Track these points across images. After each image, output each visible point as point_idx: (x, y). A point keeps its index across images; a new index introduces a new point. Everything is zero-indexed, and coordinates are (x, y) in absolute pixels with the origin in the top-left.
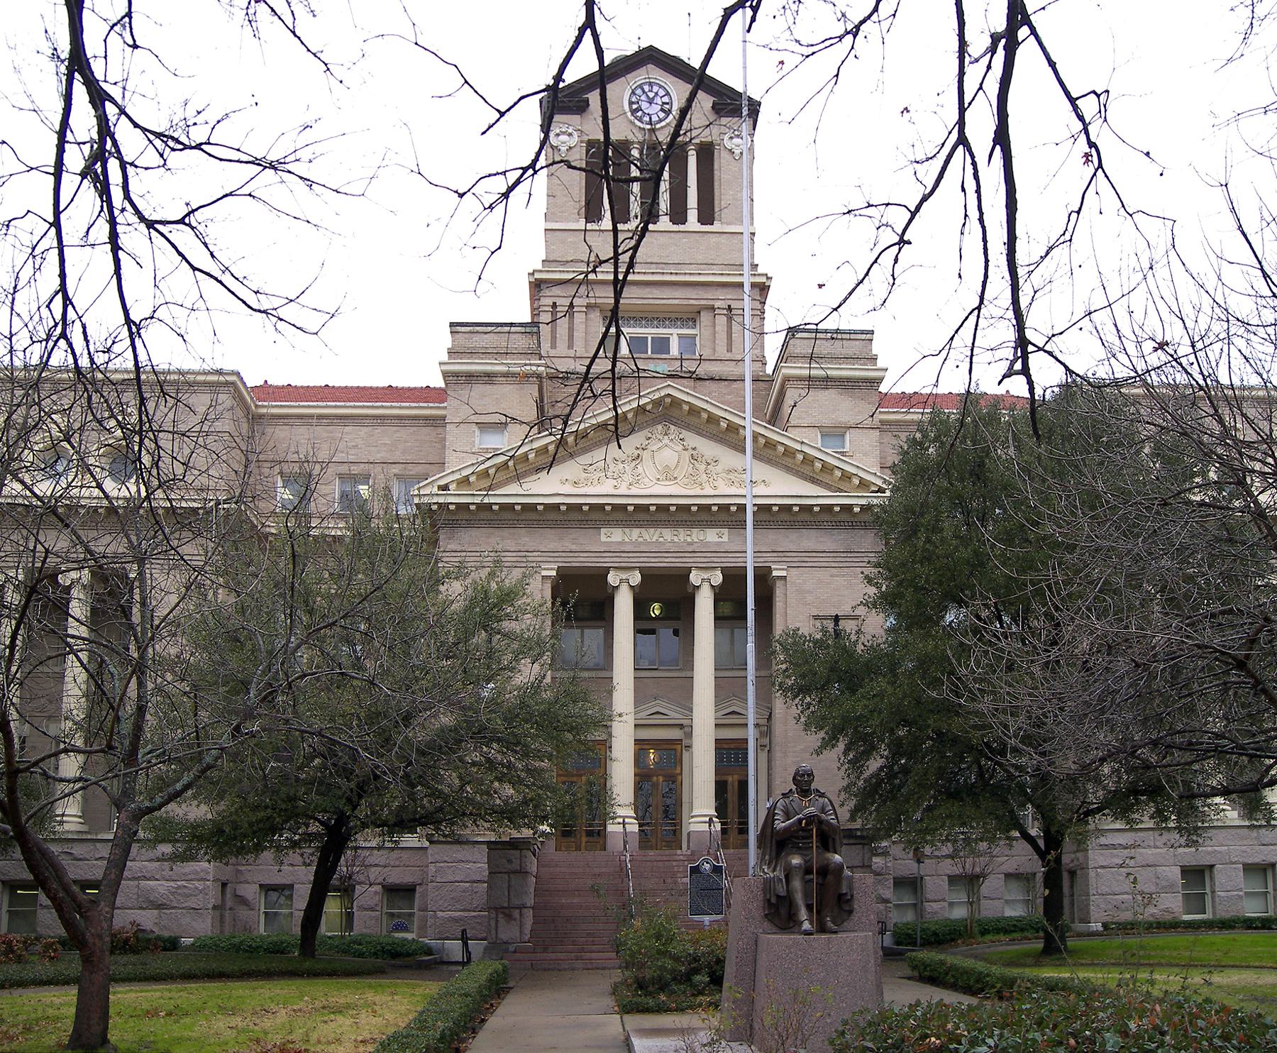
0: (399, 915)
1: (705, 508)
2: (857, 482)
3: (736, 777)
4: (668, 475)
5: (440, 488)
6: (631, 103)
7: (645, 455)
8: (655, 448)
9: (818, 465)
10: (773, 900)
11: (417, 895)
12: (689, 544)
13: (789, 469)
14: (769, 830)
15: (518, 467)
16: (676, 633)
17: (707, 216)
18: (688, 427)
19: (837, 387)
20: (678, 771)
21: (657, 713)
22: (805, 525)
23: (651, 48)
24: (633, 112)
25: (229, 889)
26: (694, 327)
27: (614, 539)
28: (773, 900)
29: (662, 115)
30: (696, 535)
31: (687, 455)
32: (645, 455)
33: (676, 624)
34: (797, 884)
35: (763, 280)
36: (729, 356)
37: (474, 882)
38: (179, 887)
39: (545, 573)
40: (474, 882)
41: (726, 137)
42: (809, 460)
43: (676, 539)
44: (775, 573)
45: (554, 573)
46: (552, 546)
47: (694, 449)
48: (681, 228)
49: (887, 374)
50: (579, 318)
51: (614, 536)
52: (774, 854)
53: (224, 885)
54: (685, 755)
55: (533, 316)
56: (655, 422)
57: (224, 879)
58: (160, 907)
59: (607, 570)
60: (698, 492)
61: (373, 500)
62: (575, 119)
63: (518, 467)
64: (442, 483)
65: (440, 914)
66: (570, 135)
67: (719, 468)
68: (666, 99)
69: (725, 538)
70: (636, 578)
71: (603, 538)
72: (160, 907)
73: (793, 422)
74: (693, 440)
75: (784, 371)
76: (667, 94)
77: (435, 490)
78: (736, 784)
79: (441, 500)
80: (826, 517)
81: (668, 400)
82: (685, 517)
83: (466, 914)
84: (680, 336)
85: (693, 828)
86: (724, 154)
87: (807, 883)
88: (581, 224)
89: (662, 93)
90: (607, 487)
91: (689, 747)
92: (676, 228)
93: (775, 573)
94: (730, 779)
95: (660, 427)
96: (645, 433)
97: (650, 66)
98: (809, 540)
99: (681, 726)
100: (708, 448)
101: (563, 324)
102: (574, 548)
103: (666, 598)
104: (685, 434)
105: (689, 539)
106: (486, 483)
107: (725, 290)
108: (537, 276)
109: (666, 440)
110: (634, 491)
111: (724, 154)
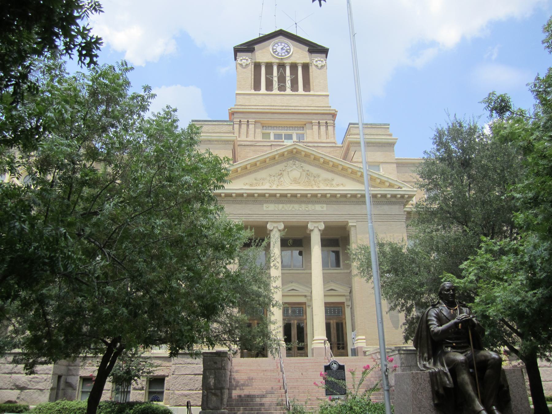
0: (155, 392)
1: (315, 196)
2: (388, 184)
3: (335, 321)
4: (295, 181)
6: (273, 49)
7: (284, 173)
8: (289, 170)
10: (441, 391)
11: (166, 382)
12: (307, 211)
13: (353, 179)
14: (424, 333)
16: (301, 253)
17: (307, 86)
18: (305, 162)
19: (374, 146)
20: (304, 317)
21: (293, 290)
23: (281, 30)
24: (274, 52)
25: (62, 379)
26: (303, 130)
27: (269, 209)
28: (441, 391)
29: (286, 53)
30: (311, 207)
31: (304, 173)
32: (284, 173)
33: (301, 249)
34: (465, 377)
35: (334, 112)
36: (319, 141)
37: (196, 375)
38: (34, 378)
40: (196, 375)
41: (314, 61)
43: (300, 209)
44: (350, 224)
46: (239, 212)
47: (308, 171)
48: (296, 93)
49: (398, 141)
50: (251, 127)
51: (270, 208)
52: (431, 352)
53: (60, 377)
54: (308, 310)
55: (230, 118)
56: (289, 159)
57: (59, 373)
58: (22, 389)
59: (267, 222)
60: (328, 188)
62: (250, 54)
65: (177, 392)
66: (247, 60)
67: (320, 179)
68: (288, 48)
69: (325, 209)
70: (282, 226)
71: (265, 208)
72: (22, 389)
73: (354, 160)
74: (307, 167)
75: (349, 139)
76: (288, 46)
78: (335, 324)
81: (295, 151)
82: (304, 199)
83: (191, 392)
84: (297, 134)
85: (314, 346)
86: (313, 67)
87: (472, 375)
88: (253, 92)
89: (286, 46)
91: (310, 306)
92: (294, 93)
93: (350, 224)
94: (332, 322)
95: (291, 162)
96: (285, 164)
97: (281, 37)
99: (305, 296)
100: (314, 170)
101: (244, 127)
102: (250, 213)
103: (295, 240)
104: (303, 164)
105: (307, 209)
107: (317, 116)
108: (232, 110)
109: (294, 167)
110: (279, 188)
111: (313, 67)
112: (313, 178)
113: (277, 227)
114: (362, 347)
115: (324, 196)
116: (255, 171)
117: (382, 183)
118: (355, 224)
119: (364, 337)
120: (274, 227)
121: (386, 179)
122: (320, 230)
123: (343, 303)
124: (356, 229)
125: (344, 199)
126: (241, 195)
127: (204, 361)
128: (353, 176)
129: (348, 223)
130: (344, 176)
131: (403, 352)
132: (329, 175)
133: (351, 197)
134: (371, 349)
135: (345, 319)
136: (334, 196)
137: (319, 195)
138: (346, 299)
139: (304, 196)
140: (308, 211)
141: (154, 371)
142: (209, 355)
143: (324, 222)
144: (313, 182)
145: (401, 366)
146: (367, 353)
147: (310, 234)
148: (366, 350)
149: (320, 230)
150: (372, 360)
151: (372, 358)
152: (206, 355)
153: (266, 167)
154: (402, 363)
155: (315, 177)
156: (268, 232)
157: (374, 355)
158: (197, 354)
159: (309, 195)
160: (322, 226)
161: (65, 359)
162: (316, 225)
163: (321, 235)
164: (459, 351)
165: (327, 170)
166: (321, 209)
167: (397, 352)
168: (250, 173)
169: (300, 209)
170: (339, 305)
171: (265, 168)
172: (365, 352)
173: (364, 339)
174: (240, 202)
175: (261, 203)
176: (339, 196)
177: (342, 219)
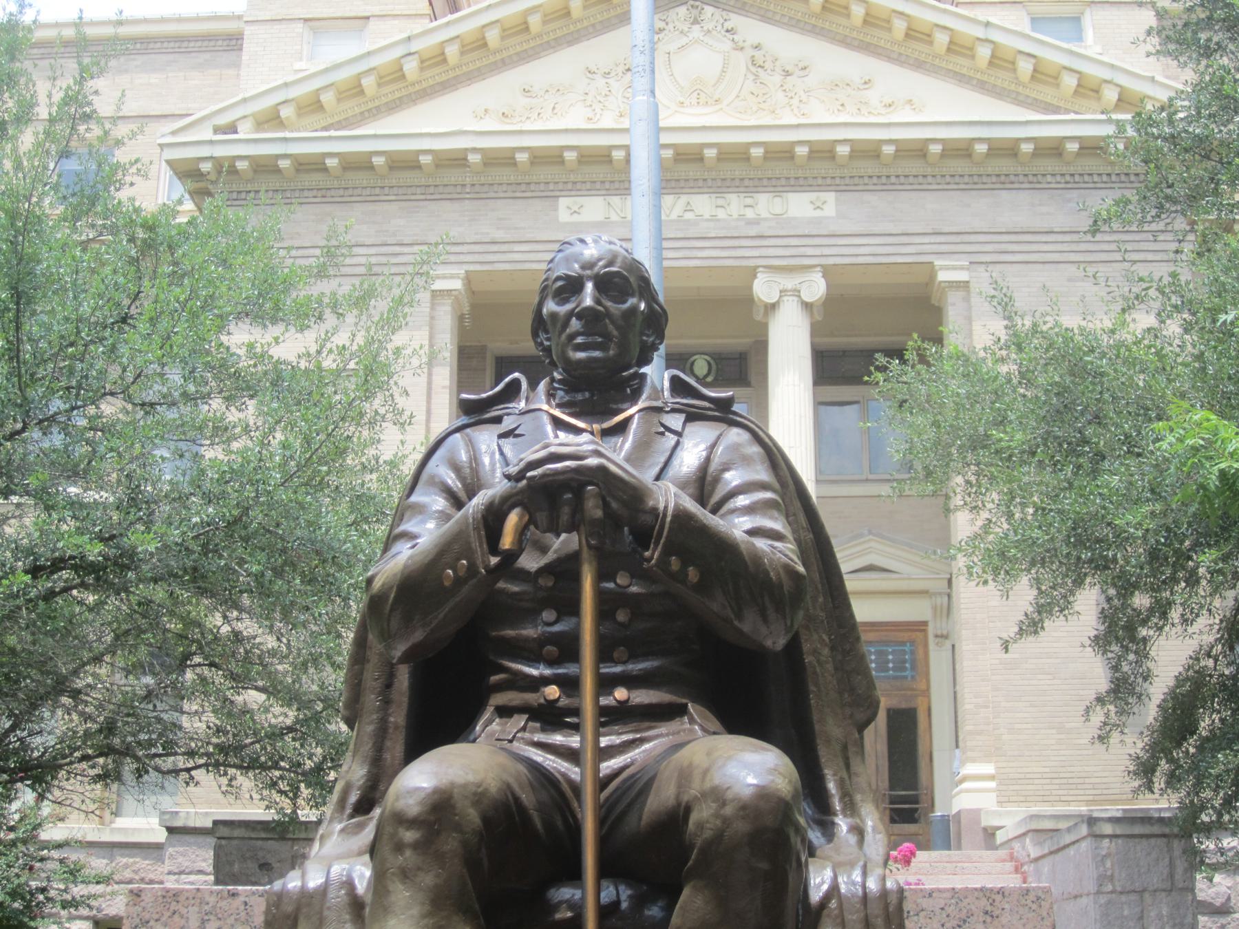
1: (781, 154)
5: (217, 130)
8: (672, 47)
9: (1025, 67)
12: (750, 223)
13: (962, 79)
15: (400, 87)
22: (1004, 182)
30: (766, 205)
31: (741, 60)
39: (439, 285)
42: (1001, 60)
43: (721, 214)
44: (942, 276)
45: (457, 285)
47: (757, 47)
54: (938, 660)
59: (753, 273)
60: (767, 120)
61: (483, 555)
63: (400, 87)
64: (223, 120)
69: (830, 210)
71: (564, 216)
77: (208, 135)
79: (220, 152)
80: (1049, 165)
90: (575, 118)
93: (942, 276)
95: (682, 10)
98: (1015, 210)
102: (500, 235)
104: (736, 20)
105: (749, 213)
106: (352, 107)
109: (696, 31)
112: (777, 78)
113: (796, 292)
114: (976, 813)
115: (823, 152)
116: (524, 57)
117: (1088, 89)
118: (962, 276)
119: (989, 769)
120: (783, 292)
121: (1105, 74)
122: (807, 306)
123: (921, 626)
124: (967, 299)
125: (914, 167)
126: (457, 160)
127: (217, 856)
128: (961, 64)
129: (931, 270)
130: (918, 65)
131: (1108, 829)
132: (852, 64)
133: (944, 155)
134: (1009, 821)
135: (926, 693)
136: (867, 152)
137: (802, 151)
138: (935, 609)
139: (735, 155)
140: (756, 222)
141: (95, 897)
142: (237, 833)
143: (827, 272)
144: (780, 94)
145: (1099, 893)
146: (1000, 837)
147: (764, 327)
148: (996, 823)
149: (807, 306)
150: (1009, 866)
151: (1012, 858)
152: (224, 831)
153: (572, 39)
154: (1102, 879)
155: (787, 74)
156: (759, 317)
157: (1017, 845)
158: (806, 861)
159: (843, 150)
160: (815, 288)
161: (293, 868)
162: (789, 282)
163: (815, 330)
164: (576, 805)
165: (845, 42)
166: (810, 212)
167: (1084, 830)
168: (503, 64)
169: (721, 214)
170: (905, 636)
171: (570, 43)
172: (989, 834)
173: (991, 778)
174: (454, 194)
175: (549, 193)
176: (889, 150)
177: (905, 254)
